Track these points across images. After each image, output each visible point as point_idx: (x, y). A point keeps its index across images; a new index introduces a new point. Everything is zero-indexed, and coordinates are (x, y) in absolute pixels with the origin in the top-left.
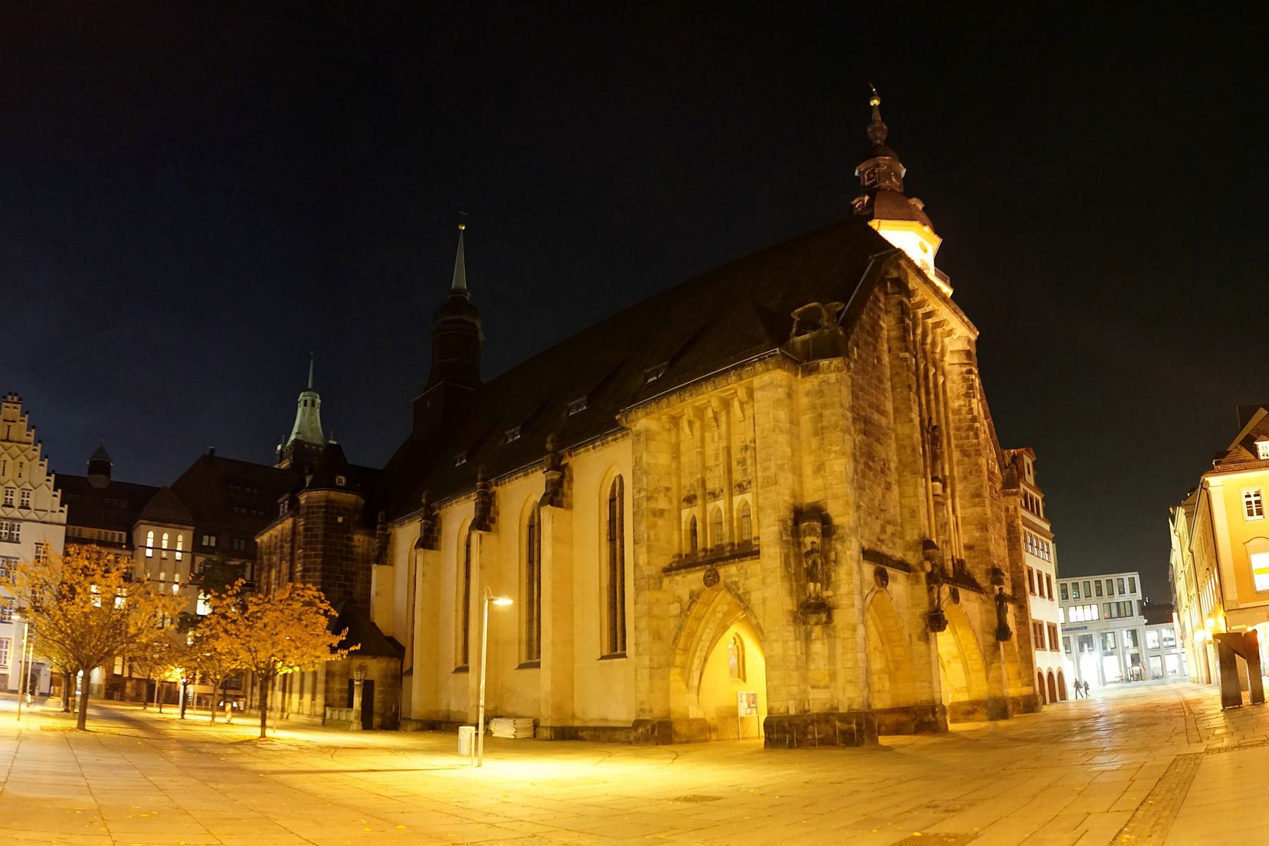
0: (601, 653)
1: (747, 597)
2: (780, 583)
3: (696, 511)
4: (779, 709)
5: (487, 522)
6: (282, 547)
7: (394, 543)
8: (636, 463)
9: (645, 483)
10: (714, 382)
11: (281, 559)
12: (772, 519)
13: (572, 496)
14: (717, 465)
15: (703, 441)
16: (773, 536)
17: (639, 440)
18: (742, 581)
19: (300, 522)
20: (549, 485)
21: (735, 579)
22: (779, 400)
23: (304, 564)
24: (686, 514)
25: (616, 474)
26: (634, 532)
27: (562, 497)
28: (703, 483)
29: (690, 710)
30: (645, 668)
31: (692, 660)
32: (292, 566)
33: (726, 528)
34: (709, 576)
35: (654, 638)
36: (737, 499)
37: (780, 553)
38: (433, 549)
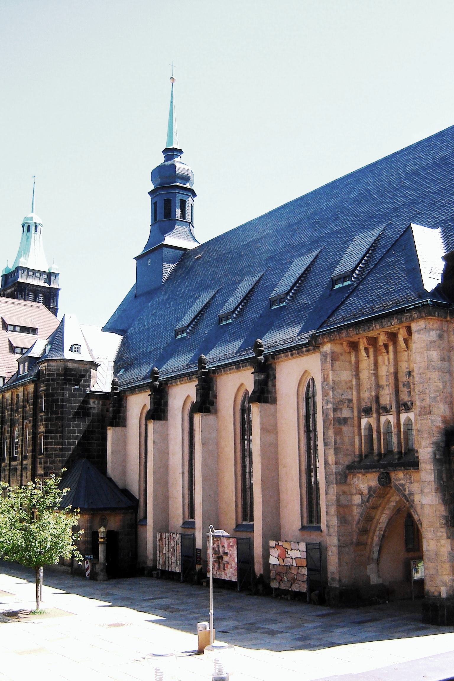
0: (302, 524)
1: (412, 498)
2: (434, 494)
3: (372, 420)
4: (433, 593)
5: (207, 405)
6: (24, 407)
7: (126, 407)
8: (324, 379)
9: (332, 397)
10: (381, 322)
11: (24, 418)
12: (428, 442)
13: (275, 392)
14: (387, 385)
15: (376, 364)
16: (429, 455)
17: (326, 359)
18: (408, 485)
19: (40, 387)
20: (257, 384)
21: (403, 482)
22: (431, 342)
23: (46, 426)
24: (364, 421)
25: (310, 377)
26: (324, 436)
27: (267, 394)
28: (377, 398)
29: (371, 578)
30: (335, 546)
31: (372, 539)
32: (35, 427)
33: (394, 439)
34: (382, 478)
35: (341, 522)
36: (403, 417)
37: (434, 470)
38: (161, 420)
